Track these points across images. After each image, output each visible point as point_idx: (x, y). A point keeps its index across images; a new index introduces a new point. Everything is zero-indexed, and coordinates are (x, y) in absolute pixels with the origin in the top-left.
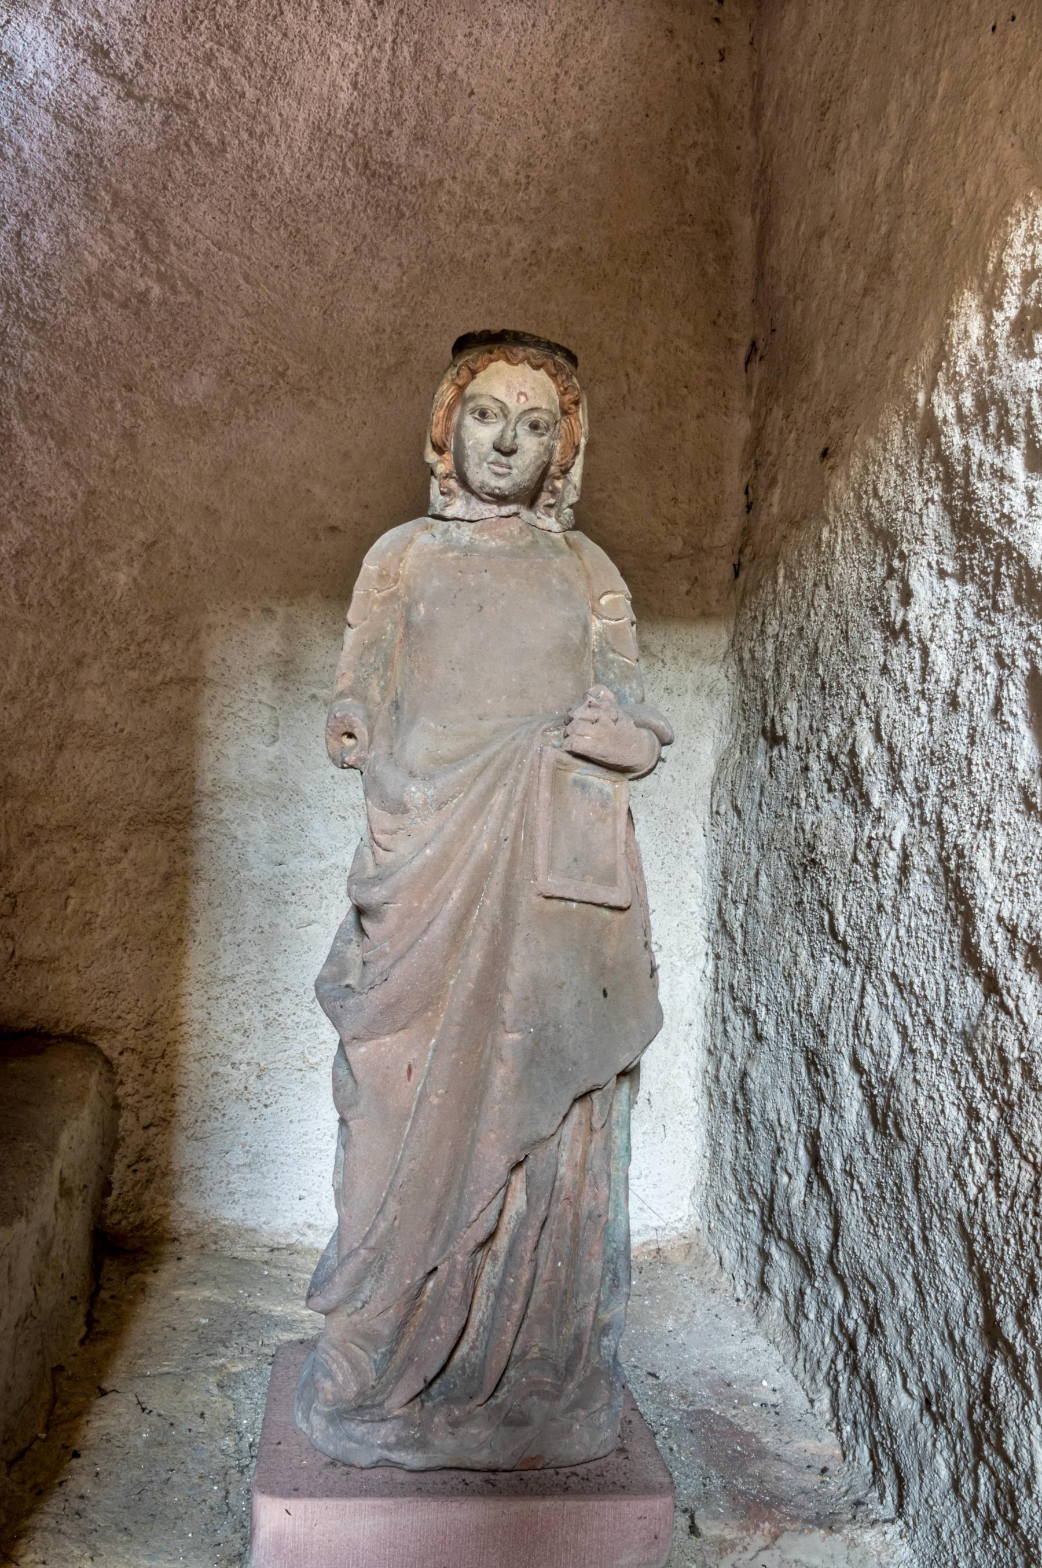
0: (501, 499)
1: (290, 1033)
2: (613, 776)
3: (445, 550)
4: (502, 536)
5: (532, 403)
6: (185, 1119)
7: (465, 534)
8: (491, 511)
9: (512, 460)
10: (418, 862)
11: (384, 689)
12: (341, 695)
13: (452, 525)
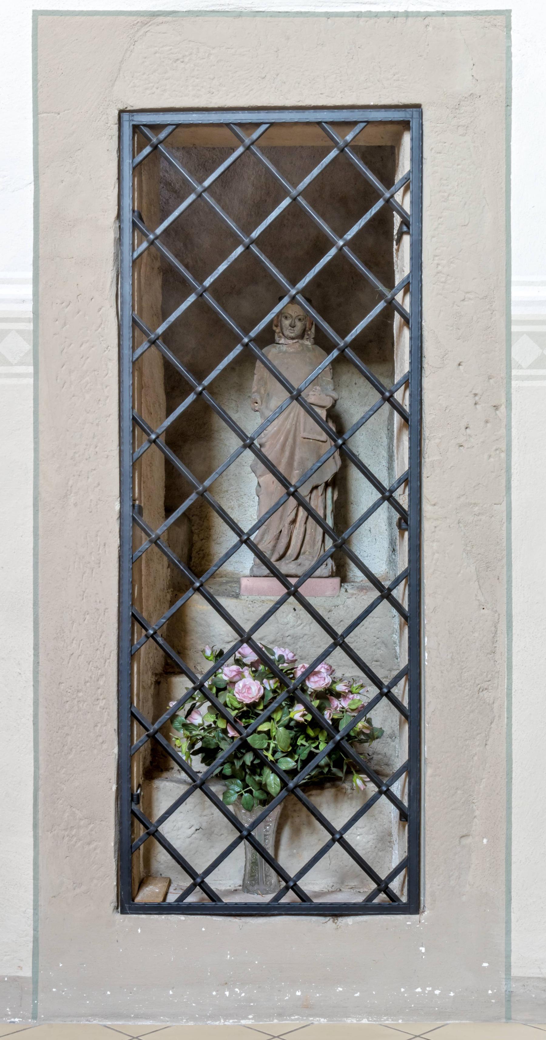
0: (293, 338)
1: (247, 509)
2: (322, 409)
3: (279, 353)
4: (294, 348)
5: (298, 314)
6: (215, 537)
7: (284, 348)
8: (290, 342)
9: (295, 329)
10: (273, 431)
11: (265, 391)
12: (254, 392)
13: (281, 345)
